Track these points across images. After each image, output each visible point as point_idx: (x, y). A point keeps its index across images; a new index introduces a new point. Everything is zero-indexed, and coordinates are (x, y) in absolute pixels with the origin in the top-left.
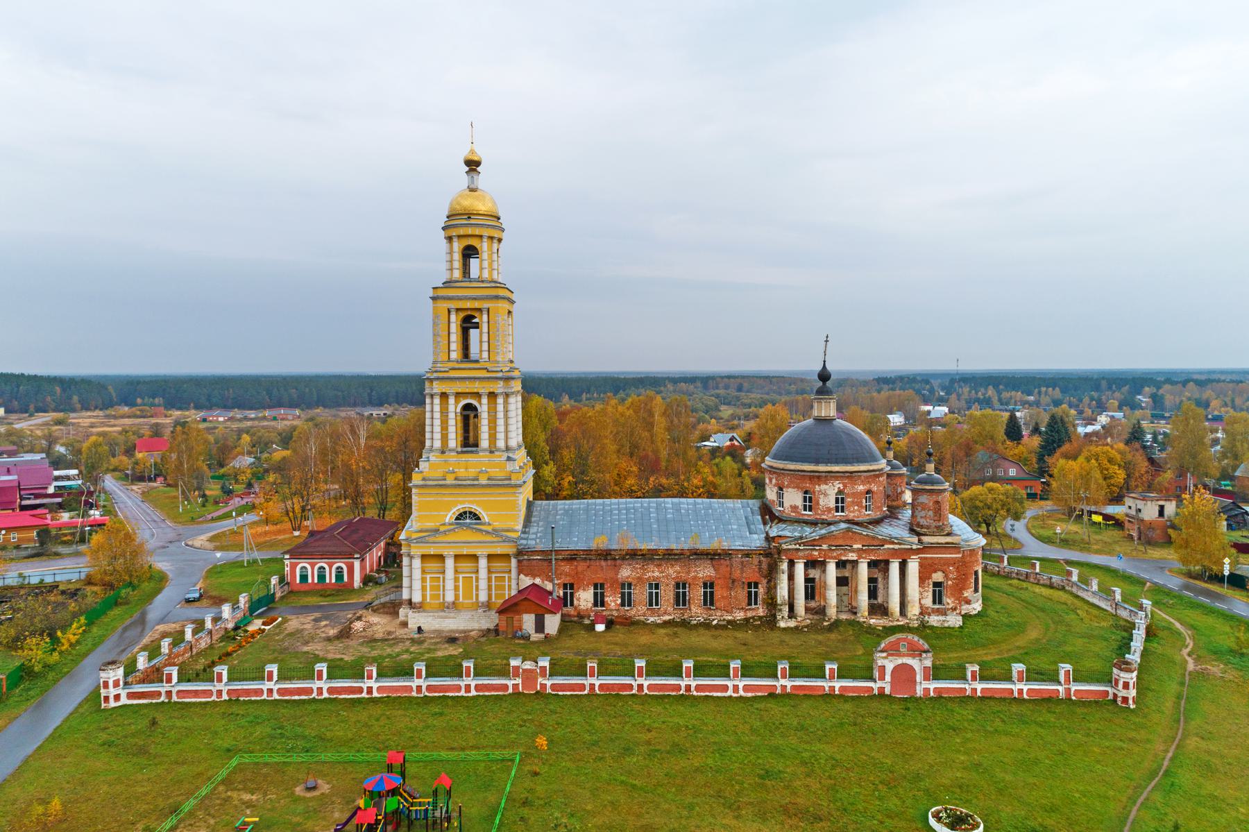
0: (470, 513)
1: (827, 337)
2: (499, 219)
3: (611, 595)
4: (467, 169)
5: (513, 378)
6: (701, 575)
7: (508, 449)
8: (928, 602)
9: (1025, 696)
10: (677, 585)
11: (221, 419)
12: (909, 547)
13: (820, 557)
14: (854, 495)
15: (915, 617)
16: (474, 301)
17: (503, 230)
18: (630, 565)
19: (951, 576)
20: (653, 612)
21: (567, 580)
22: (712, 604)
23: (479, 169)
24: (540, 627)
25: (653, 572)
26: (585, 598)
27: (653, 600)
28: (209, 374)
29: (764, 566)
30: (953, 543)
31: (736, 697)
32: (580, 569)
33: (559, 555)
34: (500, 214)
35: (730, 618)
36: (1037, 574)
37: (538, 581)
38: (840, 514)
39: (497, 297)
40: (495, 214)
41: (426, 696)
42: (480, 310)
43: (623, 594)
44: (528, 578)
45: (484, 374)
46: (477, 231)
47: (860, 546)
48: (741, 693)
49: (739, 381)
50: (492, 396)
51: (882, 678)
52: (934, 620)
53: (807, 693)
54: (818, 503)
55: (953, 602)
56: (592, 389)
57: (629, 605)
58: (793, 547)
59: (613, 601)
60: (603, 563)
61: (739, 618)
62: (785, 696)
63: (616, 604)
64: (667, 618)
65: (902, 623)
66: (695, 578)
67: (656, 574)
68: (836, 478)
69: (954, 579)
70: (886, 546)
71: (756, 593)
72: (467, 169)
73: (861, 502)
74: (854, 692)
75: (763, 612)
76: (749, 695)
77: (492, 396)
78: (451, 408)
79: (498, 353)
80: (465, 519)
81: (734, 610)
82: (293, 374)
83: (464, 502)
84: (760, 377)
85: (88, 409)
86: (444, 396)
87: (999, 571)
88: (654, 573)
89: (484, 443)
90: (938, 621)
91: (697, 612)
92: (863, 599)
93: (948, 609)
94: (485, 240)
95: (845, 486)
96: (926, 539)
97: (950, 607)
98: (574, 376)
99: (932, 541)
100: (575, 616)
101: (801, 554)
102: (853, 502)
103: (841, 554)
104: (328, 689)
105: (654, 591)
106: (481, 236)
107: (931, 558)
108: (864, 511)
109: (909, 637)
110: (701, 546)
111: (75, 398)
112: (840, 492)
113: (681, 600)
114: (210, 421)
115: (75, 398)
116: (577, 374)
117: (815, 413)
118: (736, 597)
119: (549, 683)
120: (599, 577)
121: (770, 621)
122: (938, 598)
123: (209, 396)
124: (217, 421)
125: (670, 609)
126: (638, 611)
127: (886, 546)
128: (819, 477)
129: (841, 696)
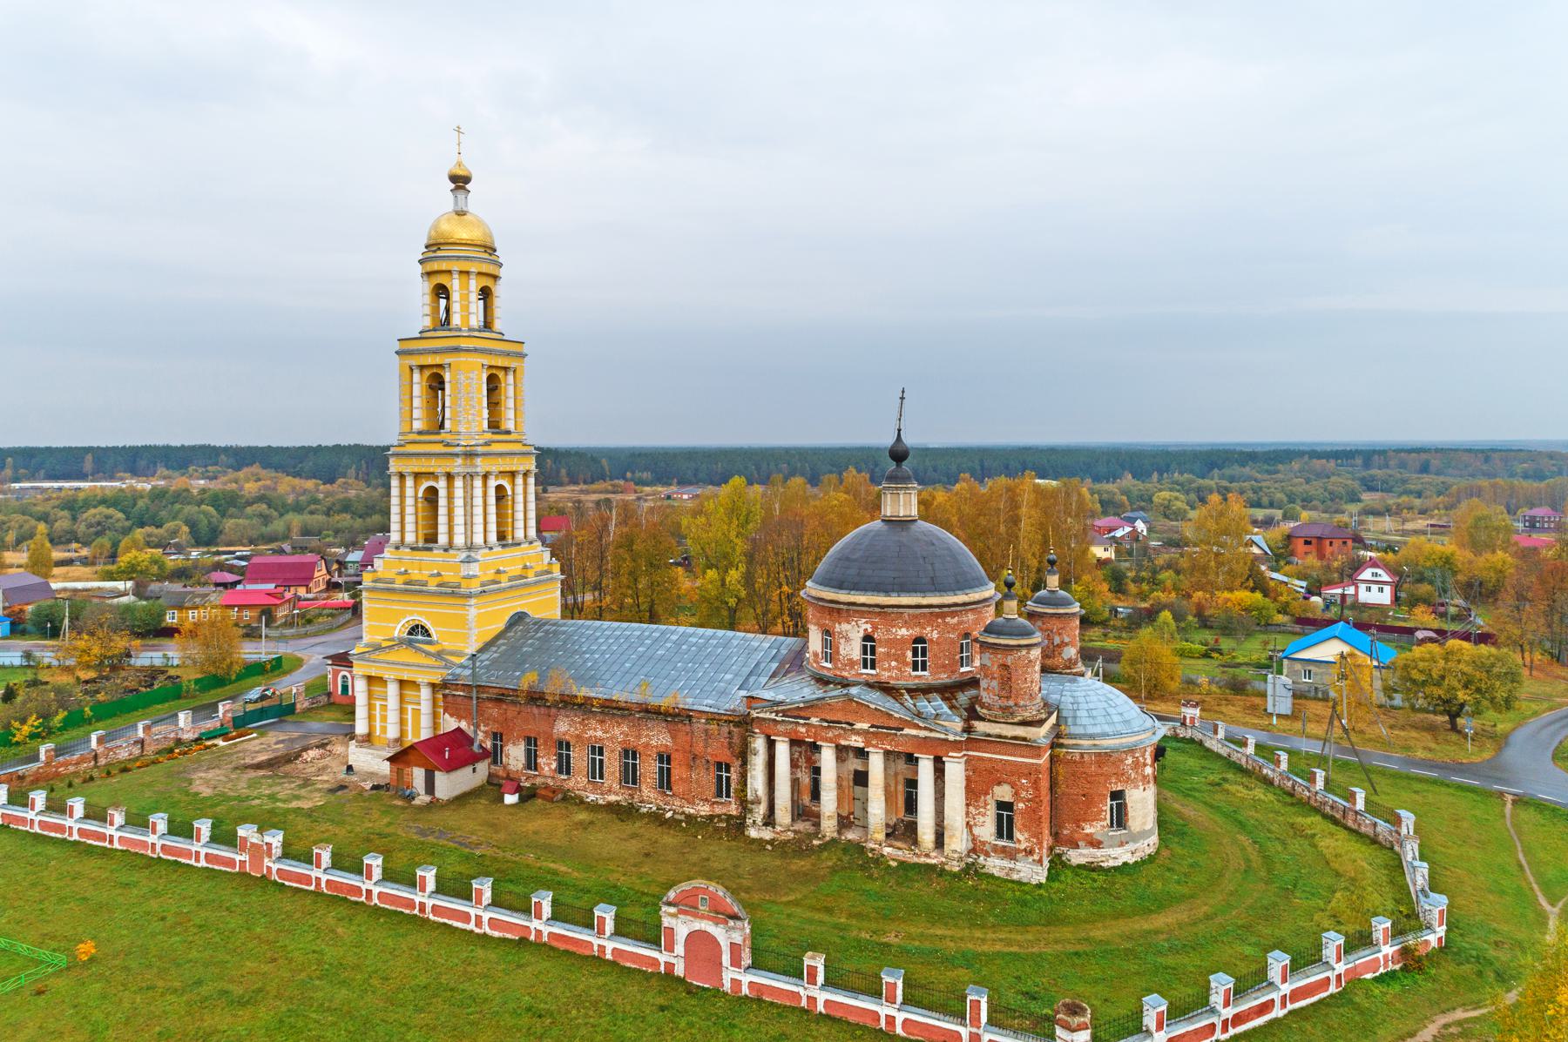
0: (423, 627)
1: (903, 392)
2: (495, 251)
3: (544, 756)
4: (453, 186)
5: (477, 455)
6: (654, 743)
7: (470, 547)
8: (987, 830)
9: (899, 1030)
10: (626, 752)
11: (685, 497)
12: (943, 736)
13: (809, 737)
14: (891, 643)
15: (956, 856)
16: (435, 355)
17: (500, 265)
18: (567, 716)
19: (1023, 794)
20: (596, 788)
21: (495, 728)
22: (670, 788)
23: (468, 186)
24: (430, 787)
25: (595, 730)
26: (515, 755)
27: (597, 770)
28: (756, 446)
29: (736, 740)
30: (1024, 739)
31: (477, 934)
32: (510, 714)
33: (483, 693)
34: (497, 245)
35: (692, 811)
36: (1356, 813)
37: (463, 725)
38: (869, 671)
39: (456, 350)
40: (488, 244)
41: (159, 858)
42: (506, 369)
43: (560, 755)
44: (453, 719)
45: (439, 448)
46: (444, 266)
47: (865, 726)
48: (486, 929)
49: (1424, 456)
50: (450, 477)
51: (670, 948)
52: (995, 865)
53: (572, 948)
54: (838, 653)
55: (1027, 840)
56: (1173, 465)
57: (568, 773)
58: (767, 716)
59: (548, 763)
60: (535, 710)
61: (703, 813)
62: (539, 946)
63: (550, 769)
64: (612, 798)
65: (934, 861)
66: (647, 745)
67: (599, 734)
68: (862, 615)
69: (1029, 800)
70: (907, 731)
71: (728, 779)
72: (453, 186)
73: (904, 655)
74: (634, 962)
75: (737, 809)
76: (496, 934)
77: (450, 477)
78: (409, 492)
79: (460, 421)
80: (417, 634)
81: (697, 802)
82: (735, 446)
83: (412, 613)
84: (1469, 451)
85: (576, 483)
86: (402, 476)
87: (1309, 798)
88: (596, 732)
89: (443, 539)
90: (1002, 869)
91: (649, 796)
92: (877, 810)
93: (1018, 851)
94: (456, 276)
95: (875, 628)
96: (980, 727)
97: (1022, 846)
98: (1205, 449)
99: (988, 731)
100: (503, 778)
101: (781, 728)
102: (888, 654)
103: (839, 736)
104: (79, 829)
105: (598, 758)
106: (450, 272)
107: (991, 759)
108: (909, 669)
109: (711, 889)
110: (654, 701)
111: (563, 472)
112: (868, 638)
113: (630, 776)
114: (674, 499)
115: (563, 472)
116: (1192, 446)
117: (888, 510)
118: (697, 781)
119: (275, 867)
120: (532, 728)
121: (737, 826)
122: (1005, 828)
123: (697, 470)
124: (681, 498)
125: (616, 786)
126: (578, 782)
127: (907, 731)
128: (839, 611)
129: (613, 963)
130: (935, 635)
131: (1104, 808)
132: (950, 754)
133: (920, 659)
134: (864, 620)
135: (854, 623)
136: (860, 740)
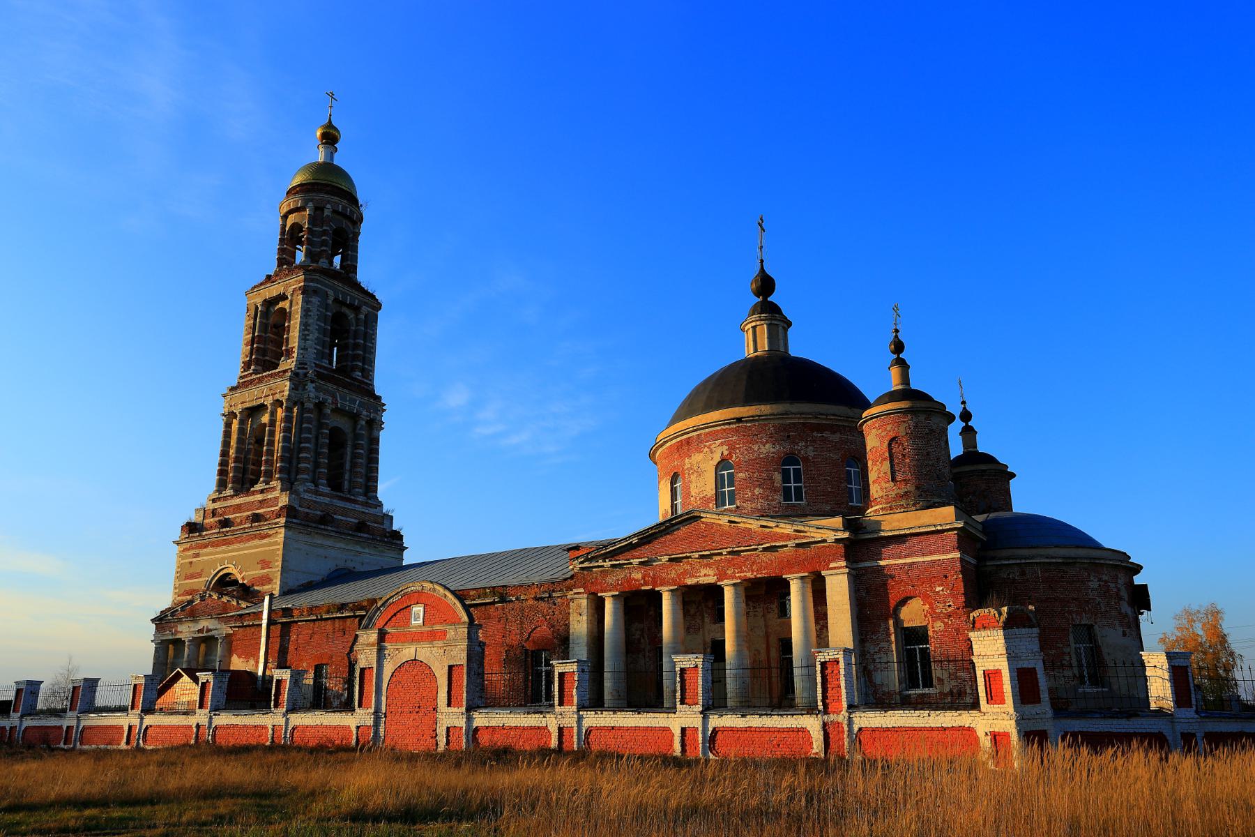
13: (646, 584)
95: (732, 448)
130: (811, 452)
131: (1067, 650)
132: (832, 565)
133: (792, 485)
134: (718, 442)
135: (706, 449)
136: (712, 573)
